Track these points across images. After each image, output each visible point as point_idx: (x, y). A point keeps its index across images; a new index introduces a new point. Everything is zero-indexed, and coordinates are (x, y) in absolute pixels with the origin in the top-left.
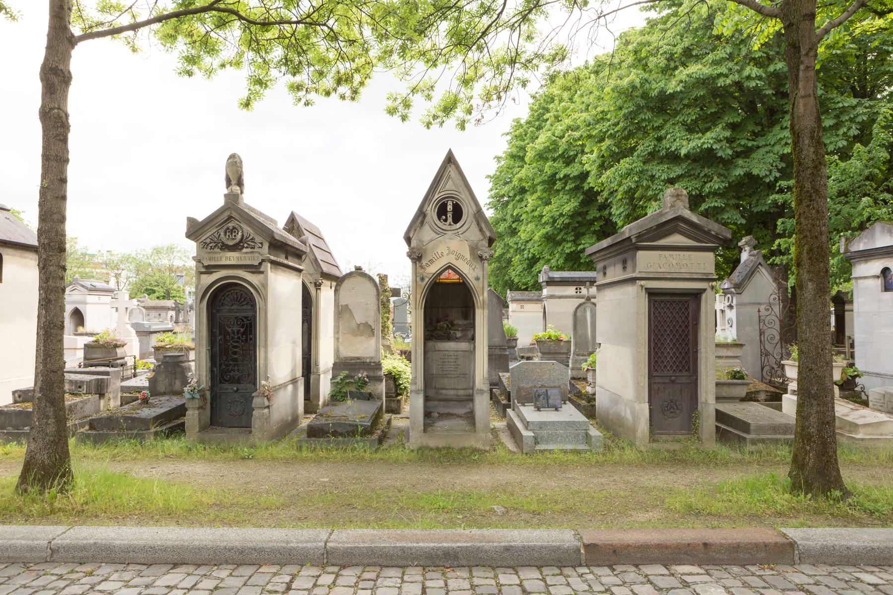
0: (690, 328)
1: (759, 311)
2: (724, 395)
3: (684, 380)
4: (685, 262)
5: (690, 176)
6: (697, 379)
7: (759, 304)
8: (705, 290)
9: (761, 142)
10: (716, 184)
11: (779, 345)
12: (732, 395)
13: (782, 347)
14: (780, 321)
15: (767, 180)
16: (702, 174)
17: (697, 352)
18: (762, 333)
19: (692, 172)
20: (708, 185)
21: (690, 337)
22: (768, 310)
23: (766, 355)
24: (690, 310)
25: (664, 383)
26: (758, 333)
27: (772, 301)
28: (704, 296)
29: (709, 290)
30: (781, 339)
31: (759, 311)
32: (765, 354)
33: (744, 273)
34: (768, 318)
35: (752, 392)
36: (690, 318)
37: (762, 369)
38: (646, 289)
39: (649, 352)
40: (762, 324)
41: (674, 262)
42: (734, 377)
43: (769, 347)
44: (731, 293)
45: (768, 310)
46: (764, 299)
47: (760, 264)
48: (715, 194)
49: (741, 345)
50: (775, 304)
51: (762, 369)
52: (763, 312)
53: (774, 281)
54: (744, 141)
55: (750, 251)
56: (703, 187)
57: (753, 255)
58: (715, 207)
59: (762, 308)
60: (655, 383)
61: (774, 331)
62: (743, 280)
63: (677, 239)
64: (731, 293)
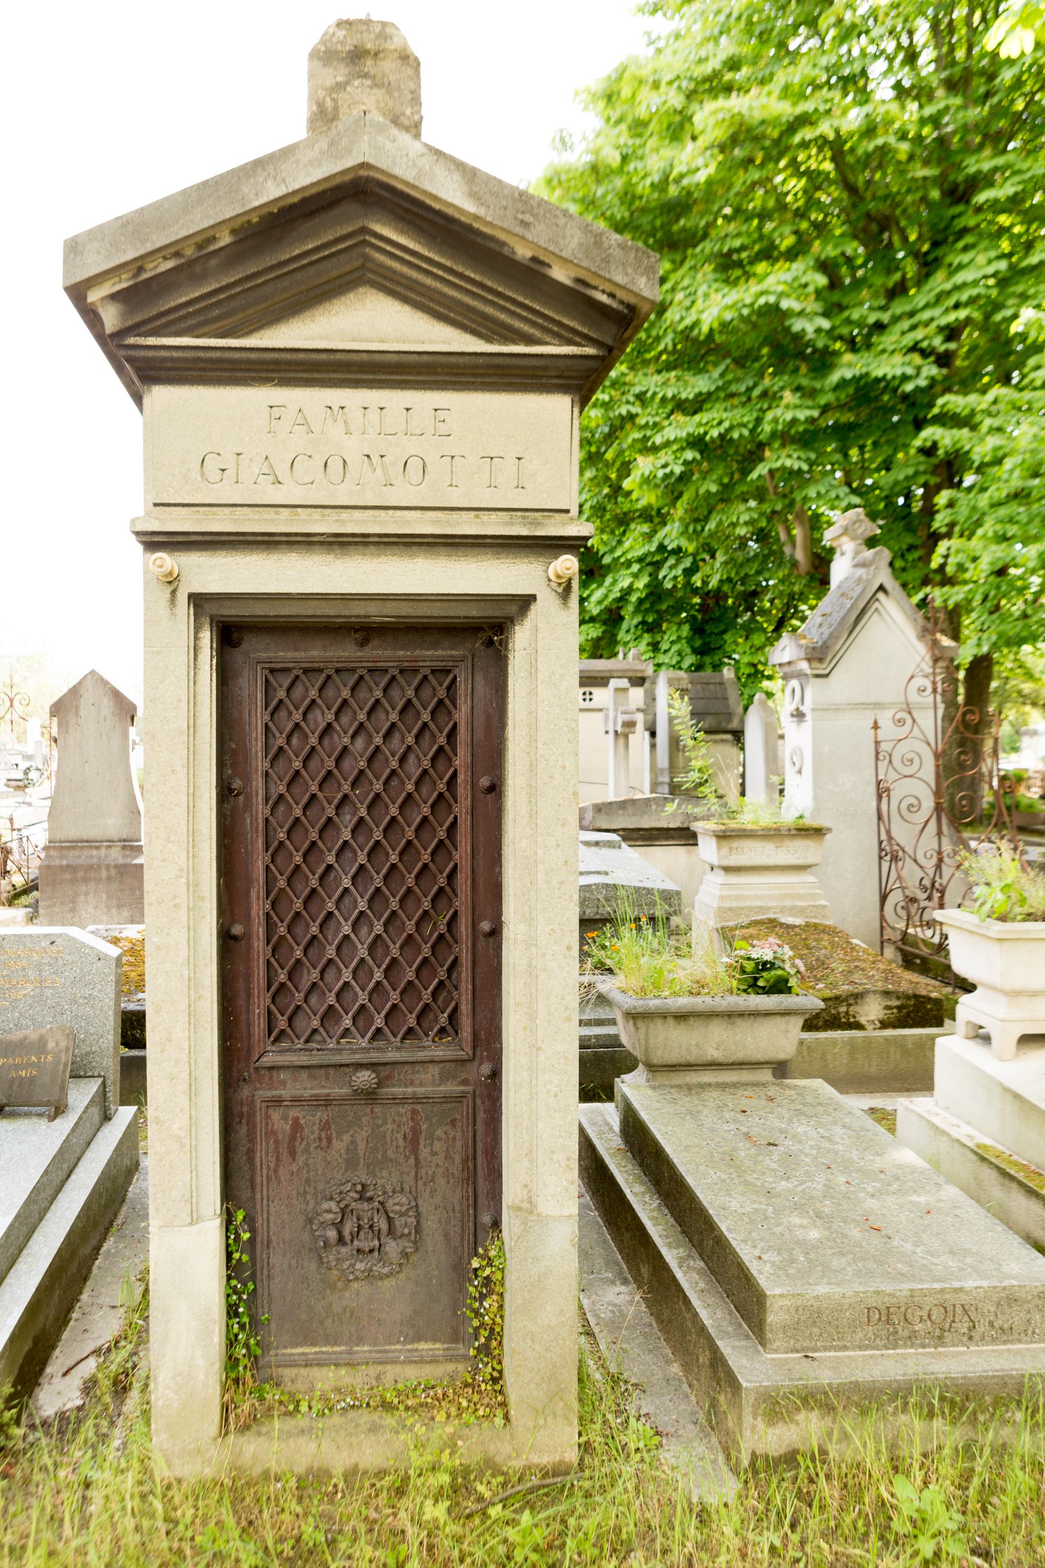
0: (462, 808)
1: (876, 727)
2: (713, 1053)
3: (428, 1084)
4: (411, 447)
5: (732, 395)
6: (496, 1074)
7: (878, 706)
8: (526, 602)
9: (899, 307)
10: (790, 409)
11: (933, 825)
12: (740, 1056)
13: (940, 833)
14: (937, 756)
15: (909, 387)
16: (756, 393)
17: (496, 932)
18: (882, 792)
19: (733, 388)
20: (769, 416)
21: (462, 854)
22: (901, 722)
23: (895, 858)
24: (462, 714)
25: (327, 1102)
26: (872, 789)
27: (913, 697)
28: (521, 637)
29: (546, 604)
30: (938, 808)
31: (876, 727)
32: (889, 853)
33: (837, 617)
34: (902, 749)
35: (837, 999)
36: (462, 759)
37: (883, 898)
38: (198, 600)
39: (229, 943)
40: (883, 766)
41: (353, 449)
42: (753, 986)
43: (902, 834)
44: (800, 675)
45: (901, 722)
46: (892, 694)
47: (881, 588)
48: (786, 437)
49: (818, 832)
50: (922, 707)
51: (883, 898)
52: (888, 731)
53: (921, 637)
54: (865, 310)
55: (857, 553)
56: (759, 421)
57: (863, 565)
58: (783, 468)
59: (885, 719)
60: (277, 1102)
61: (918, 786)
62: (833, 637)
63: (369, 321)
64: (800, 675)
